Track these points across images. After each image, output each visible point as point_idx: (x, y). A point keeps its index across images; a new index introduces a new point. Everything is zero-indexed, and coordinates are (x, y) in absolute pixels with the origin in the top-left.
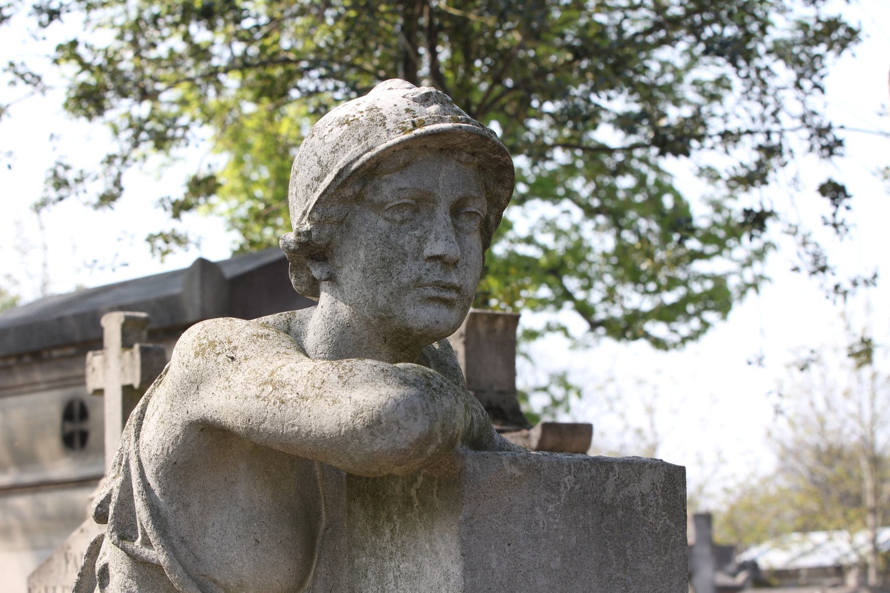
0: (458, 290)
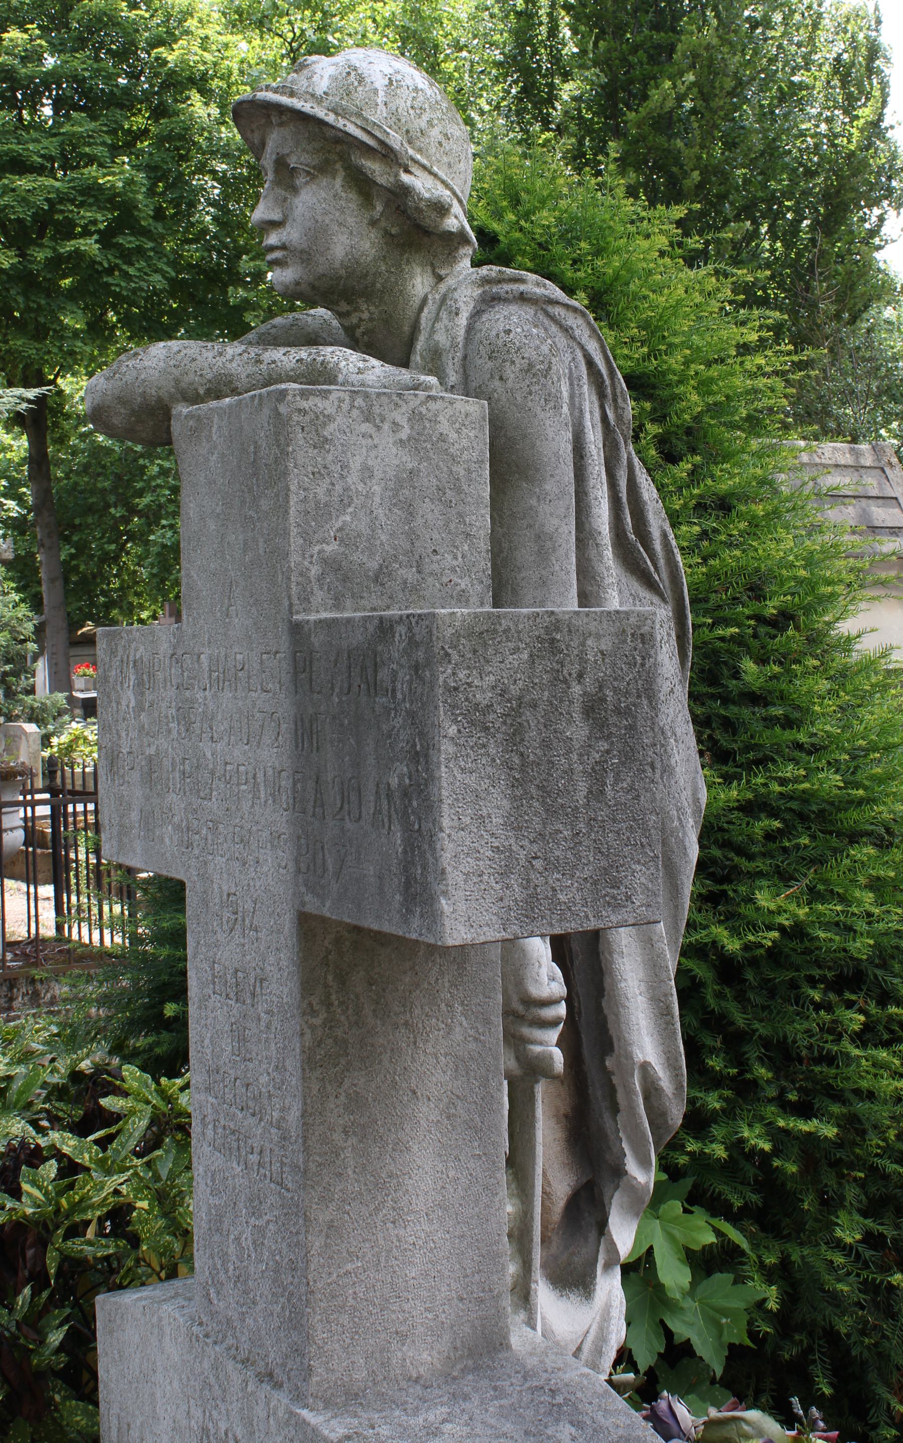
0: (283, 247)
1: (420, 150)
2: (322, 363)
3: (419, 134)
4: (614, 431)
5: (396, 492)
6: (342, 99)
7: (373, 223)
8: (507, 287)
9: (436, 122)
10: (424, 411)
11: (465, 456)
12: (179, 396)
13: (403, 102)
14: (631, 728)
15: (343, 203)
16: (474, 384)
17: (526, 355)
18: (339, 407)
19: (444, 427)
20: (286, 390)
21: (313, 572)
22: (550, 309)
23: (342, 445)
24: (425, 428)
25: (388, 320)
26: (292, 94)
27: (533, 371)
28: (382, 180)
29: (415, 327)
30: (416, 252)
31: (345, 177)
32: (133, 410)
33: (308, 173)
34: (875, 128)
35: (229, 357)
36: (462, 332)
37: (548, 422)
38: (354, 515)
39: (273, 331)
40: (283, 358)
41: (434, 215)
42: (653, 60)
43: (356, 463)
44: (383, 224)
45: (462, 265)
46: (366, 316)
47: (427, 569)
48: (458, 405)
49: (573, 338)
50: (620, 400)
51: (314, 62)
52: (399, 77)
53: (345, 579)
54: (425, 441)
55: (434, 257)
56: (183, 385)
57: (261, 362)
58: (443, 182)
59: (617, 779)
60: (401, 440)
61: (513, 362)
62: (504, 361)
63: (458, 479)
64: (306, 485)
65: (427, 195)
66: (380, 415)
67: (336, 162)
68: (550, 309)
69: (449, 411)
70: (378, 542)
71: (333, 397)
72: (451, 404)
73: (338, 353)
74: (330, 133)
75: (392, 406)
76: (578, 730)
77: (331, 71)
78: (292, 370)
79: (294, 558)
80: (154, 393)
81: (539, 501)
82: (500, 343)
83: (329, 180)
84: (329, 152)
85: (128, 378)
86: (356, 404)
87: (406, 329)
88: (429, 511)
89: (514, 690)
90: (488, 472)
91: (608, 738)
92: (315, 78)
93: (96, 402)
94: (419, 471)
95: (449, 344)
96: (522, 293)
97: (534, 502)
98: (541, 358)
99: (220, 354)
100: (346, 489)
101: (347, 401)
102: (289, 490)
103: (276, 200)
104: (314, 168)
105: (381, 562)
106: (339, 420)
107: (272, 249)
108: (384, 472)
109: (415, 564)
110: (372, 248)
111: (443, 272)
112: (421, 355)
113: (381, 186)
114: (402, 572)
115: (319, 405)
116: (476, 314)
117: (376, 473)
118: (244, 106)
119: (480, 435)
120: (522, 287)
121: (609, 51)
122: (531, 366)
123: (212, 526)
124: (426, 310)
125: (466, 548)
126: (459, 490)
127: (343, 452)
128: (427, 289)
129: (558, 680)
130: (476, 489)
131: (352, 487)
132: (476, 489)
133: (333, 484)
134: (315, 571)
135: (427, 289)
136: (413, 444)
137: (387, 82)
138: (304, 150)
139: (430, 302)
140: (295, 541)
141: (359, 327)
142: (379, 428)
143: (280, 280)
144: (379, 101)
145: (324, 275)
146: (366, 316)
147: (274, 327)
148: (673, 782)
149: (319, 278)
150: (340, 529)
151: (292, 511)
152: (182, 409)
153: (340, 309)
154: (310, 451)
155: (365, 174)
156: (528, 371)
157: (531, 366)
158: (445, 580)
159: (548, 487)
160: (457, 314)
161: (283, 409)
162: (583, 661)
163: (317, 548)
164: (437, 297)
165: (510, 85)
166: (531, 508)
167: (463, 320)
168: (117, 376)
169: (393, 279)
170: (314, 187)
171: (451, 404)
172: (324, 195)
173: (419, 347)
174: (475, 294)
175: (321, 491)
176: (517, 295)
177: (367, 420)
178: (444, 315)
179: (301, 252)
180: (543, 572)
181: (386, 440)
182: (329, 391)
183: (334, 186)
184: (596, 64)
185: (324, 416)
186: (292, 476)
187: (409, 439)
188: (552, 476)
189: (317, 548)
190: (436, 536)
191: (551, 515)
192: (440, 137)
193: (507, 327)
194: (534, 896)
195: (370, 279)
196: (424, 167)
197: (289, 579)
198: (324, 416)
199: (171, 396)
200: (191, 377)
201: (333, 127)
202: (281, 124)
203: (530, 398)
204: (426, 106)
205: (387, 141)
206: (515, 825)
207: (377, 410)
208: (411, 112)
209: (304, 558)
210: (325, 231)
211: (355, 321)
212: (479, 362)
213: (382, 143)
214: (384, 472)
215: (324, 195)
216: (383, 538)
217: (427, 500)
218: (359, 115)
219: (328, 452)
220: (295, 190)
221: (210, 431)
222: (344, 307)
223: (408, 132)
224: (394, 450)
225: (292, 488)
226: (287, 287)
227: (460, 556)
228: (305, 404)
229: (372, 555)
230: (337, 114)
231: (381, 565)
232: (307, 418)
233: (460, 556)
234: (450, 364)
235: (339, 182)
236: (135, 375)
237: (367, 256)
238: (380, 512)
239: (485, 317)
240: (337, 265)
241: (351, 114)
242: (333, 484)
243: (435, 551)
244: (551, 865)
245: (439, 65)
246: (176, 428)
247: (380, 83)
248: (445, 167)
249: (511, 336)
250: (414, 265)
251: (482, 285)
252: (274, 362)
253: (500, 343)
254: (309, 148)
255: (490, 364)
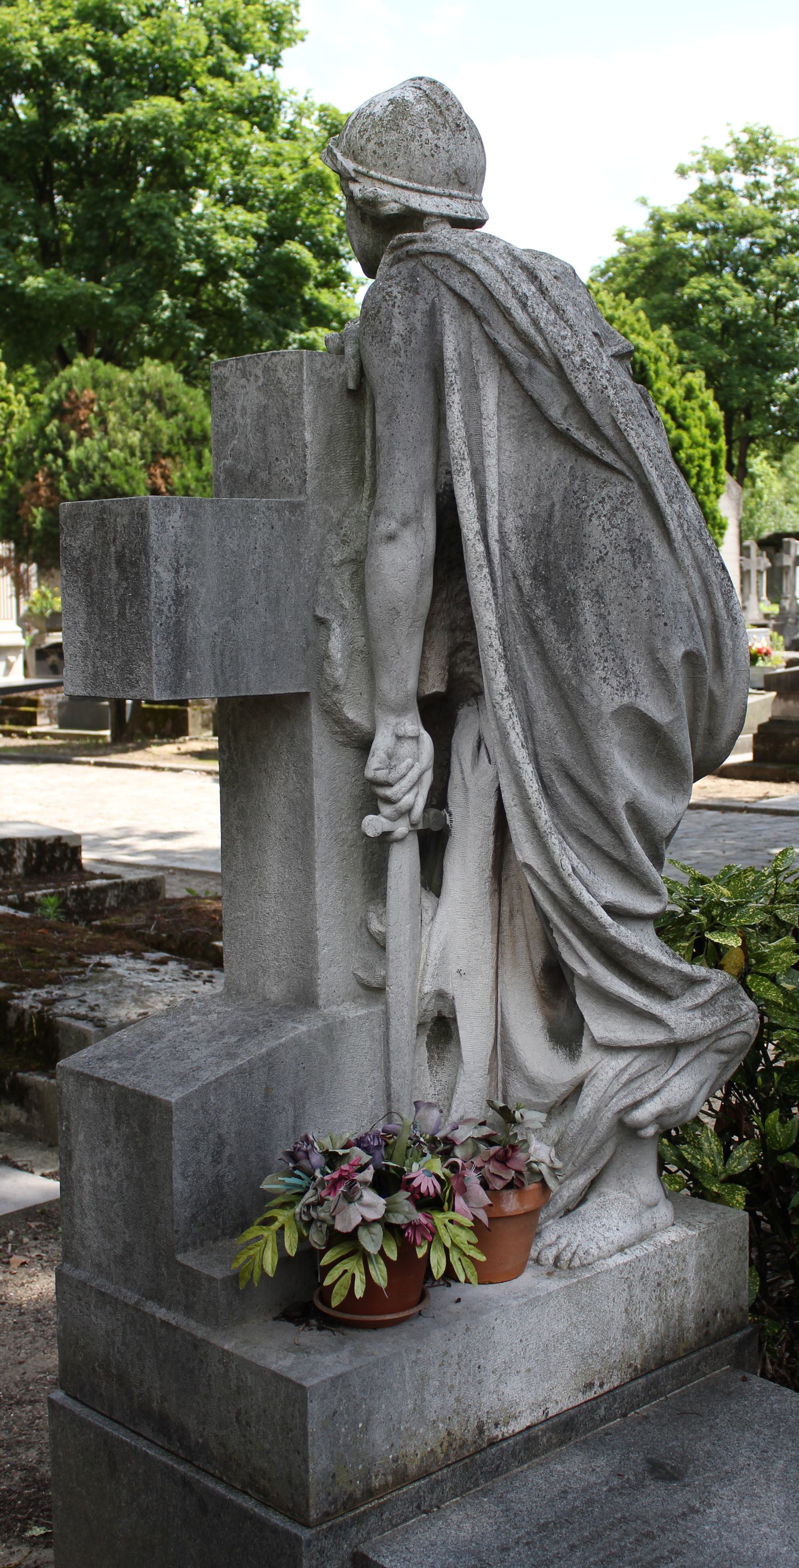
14: (137, 574)
37: (374, 354)
59: (131, 607)
69: (283, 362)
71: (228, 365)
76: (113, 575)
88: (274, 432)
89: (88, 548)
91: (126, 579)
129: (105, 544)
148: (580, 637)
150: (232, 450)
162: (116, 531)
181: (252, 388)
194: (96, 672)
206: (89, 629)
207: (248, 369)
244: (104, 657)
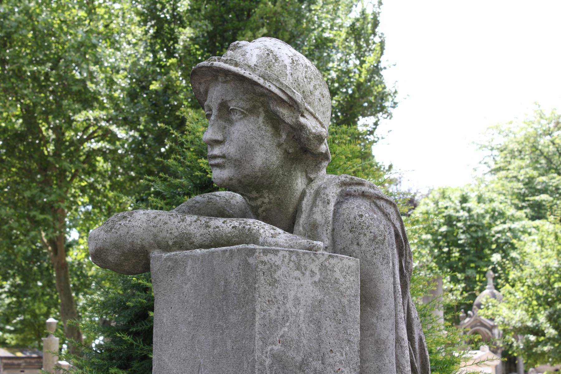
0: (223, 157)
1: (309, 103)
2: (249, 229)
3: (309, 94)
4: (406, 276)
5: (312, 313)
6: (266, 69)
7: (279, 145)
8: (355, 188)
9: (317, 86)
10: (327, 265)
11: (348, 292)
12: (156, 245)
13: (300, 74)
15: (263, 132)
16: (340, 247)
17: (372, 231)
18: (283, 261)
19: (337, 274)
20: (255, 249)
21: (267, 363)
22: (378, 202)
23: (284, 284)
24: (327, 275)
25: (280, 204)
26: (236, 65)
27: (377, 241)
28: (288, 120)
29: (297, 210)
30: (299, 164)
31: (264, 118)
32: (124, 253)
33: (243, 113)
34: (376, 70)
35: (188, 222)
36: (331, 215)
37: (384, 272)
38: (289, 327)
39: (197, 205)
40: (223, 225)
41: (316, 142)
42: (239, 17)
43: (291, 296)
44: (284, 146)
45: (322, 172)
46: (266, 200)
47: (329, 361)
48: (345, 261)
49: (390, 220)
50: (408, 258)
51: (244, 45)
52: (297, 59)
53: (284, 367)
54: (327, 283)
55: (307, 166)
56: (159, 238)
57: (209, 227)
58: (320, 123)
60: (315, 282)
61: (365, 235)
62: (360, 234)
63: (344, 306)
64: (265, 308)
65: (314, 131)
66: (305, 266)
67: (260, 107)
68: (378, 202)
69: (340, 265)
70: (302, 345)
71: (280, 254)
72: (341, 260)
73: (257, 223)
74: (259, 90)
75: (311, 260)
77: (257, 52)
78: (229, 233)
79: (258, 354)
80: (139, 242)
81: (377, 320)
82: (357, 222)
83: (255, 118)
84: (256, 101)
85: (122, 232)
86: (292, 259)
87: (291, 210)
88: (328, 325)
90: (359, 302)
92: (248, 56)
93: (98, 246)
94: (324, 301)
95: (323, 221)
96: (363, 192)
97: (374, 320)
98: (380, 233)
99: (183, 220)
100: (286, 311)
101: (287, 257)
102: (255, 311)
103: (219, 127)
104: (247, 110)
105: (303, 357)
106: (283, 268)
107: (215, 157)
108: (306, 301)
109: (320, 358)
110: (277, 160)
111: (312, 176)
112: (303, 227)
113: (288, 124)
114: (314, 363)
115: (273, 259)
116: (338, 204)
117: (301, 302)
118: (203, 69)
119: (356, 280)
120: (363, 188)
121: (213, 10)
122: (375, 237)
123: (184, 329)
124: (305, 199)
125: (348, 349)
126: (344, 313)
127: (285, 288)
128: (304, 186)
130: (353, 313)
131: (289, 310)
132: (353, 313)
133: (279, 308)
134: (268, 362)
135: (304, 186)
136: (321, 284)
137: (291, 61)
138: (241, 99)
139: (308, 194)
140: (258, 344)
141: (261, 207)
142: (303, 274)
143: (219, 176)
144: (288, 72)
145: (247, 175)
146: (266, 200)
147: (197, 202)
149: (245, 177)
150: (282, 336)
151: (257, 324)
152: (155, 254)
153: (251, 196)
154: (267, 287)
155: (278, 116)
156: (374, 240)
157: (375, 237)
158: (336, 368)
159: (382, 311)
160: (328, 203)
161: (251, 260)
163: (269, 348)
164: (312, 192)
165: (149, 29)
166: (373, 324)
167: (331, 207)
168: (113, 230)
169: (285, 180)
170: (246, 121)
171: (341, 260)
172: (252, 127)
173: (301, 222)
174: (337, 192)
175: (272, 312)
176: (361, 193)
177: (298, 269)
178: (319, 203)
179: (235, 160)
180: (379, 364)
181: (307, 281)
182: (278, 251)
183: (258, 122)
184: (205, 18)
185: (275, 266)
186: (257, 302)
187: (319, 280)
188: (385, 304)
189: (269, 348)
190: (332, 341)
191: (384, 328)
192: (320, 96)
193: (360, 213)
195: (273, 179)
196: (311, 114)
197: (254, 367)
198: (275, 266)
199: (151, 245)
200: (164, 233)
201: (262, 87)
202: (224, 82)
203: (375, 257)
204: (312, 77)
205: (294, 97)
207: (303, 263)
208: (305, 80)
209: (263, 354)
210: (252, 149)
211: (259, 202)
212: (344, 233)
213: (290, 98)
214: (306, 301)
215: (252, 127)
216: (305, 342)
217: (328, 319)
218: (278, 80)
219: (277, 288)
220: (231, 122)
221: (185, 270)
222: (254, 194)
223: (304, 92)
224: (311, 288)
225: (257, 310)
226: (224, 181)
227: (344, 354)
228: (265, 258)
229: (299, 352)
230: (264, 79)
231: (303, 359)
232: (266, 267)
233: (344, 354)
234: (325, 233)
235: (261, 119)
236: (126, 230)
237: (274, 165)
238: (303, 326)
239: (344, 206)
240: (257, 169)
241: (273, 80)
242: (279, 308)
243: (331, 350)
245: (95, 9)
246: (155, 266)
247: (288, 62)
248: (321, 114)
249: (363, 218)
250: (298, 171)
251: (341, 186)
252: (218, 227)
253: (357, 222)
254: (244, 98)
255: (351, 235)
